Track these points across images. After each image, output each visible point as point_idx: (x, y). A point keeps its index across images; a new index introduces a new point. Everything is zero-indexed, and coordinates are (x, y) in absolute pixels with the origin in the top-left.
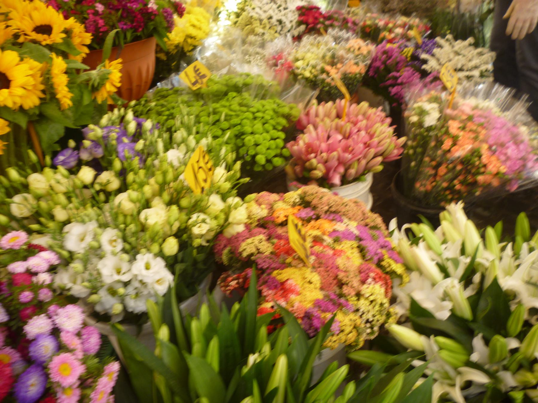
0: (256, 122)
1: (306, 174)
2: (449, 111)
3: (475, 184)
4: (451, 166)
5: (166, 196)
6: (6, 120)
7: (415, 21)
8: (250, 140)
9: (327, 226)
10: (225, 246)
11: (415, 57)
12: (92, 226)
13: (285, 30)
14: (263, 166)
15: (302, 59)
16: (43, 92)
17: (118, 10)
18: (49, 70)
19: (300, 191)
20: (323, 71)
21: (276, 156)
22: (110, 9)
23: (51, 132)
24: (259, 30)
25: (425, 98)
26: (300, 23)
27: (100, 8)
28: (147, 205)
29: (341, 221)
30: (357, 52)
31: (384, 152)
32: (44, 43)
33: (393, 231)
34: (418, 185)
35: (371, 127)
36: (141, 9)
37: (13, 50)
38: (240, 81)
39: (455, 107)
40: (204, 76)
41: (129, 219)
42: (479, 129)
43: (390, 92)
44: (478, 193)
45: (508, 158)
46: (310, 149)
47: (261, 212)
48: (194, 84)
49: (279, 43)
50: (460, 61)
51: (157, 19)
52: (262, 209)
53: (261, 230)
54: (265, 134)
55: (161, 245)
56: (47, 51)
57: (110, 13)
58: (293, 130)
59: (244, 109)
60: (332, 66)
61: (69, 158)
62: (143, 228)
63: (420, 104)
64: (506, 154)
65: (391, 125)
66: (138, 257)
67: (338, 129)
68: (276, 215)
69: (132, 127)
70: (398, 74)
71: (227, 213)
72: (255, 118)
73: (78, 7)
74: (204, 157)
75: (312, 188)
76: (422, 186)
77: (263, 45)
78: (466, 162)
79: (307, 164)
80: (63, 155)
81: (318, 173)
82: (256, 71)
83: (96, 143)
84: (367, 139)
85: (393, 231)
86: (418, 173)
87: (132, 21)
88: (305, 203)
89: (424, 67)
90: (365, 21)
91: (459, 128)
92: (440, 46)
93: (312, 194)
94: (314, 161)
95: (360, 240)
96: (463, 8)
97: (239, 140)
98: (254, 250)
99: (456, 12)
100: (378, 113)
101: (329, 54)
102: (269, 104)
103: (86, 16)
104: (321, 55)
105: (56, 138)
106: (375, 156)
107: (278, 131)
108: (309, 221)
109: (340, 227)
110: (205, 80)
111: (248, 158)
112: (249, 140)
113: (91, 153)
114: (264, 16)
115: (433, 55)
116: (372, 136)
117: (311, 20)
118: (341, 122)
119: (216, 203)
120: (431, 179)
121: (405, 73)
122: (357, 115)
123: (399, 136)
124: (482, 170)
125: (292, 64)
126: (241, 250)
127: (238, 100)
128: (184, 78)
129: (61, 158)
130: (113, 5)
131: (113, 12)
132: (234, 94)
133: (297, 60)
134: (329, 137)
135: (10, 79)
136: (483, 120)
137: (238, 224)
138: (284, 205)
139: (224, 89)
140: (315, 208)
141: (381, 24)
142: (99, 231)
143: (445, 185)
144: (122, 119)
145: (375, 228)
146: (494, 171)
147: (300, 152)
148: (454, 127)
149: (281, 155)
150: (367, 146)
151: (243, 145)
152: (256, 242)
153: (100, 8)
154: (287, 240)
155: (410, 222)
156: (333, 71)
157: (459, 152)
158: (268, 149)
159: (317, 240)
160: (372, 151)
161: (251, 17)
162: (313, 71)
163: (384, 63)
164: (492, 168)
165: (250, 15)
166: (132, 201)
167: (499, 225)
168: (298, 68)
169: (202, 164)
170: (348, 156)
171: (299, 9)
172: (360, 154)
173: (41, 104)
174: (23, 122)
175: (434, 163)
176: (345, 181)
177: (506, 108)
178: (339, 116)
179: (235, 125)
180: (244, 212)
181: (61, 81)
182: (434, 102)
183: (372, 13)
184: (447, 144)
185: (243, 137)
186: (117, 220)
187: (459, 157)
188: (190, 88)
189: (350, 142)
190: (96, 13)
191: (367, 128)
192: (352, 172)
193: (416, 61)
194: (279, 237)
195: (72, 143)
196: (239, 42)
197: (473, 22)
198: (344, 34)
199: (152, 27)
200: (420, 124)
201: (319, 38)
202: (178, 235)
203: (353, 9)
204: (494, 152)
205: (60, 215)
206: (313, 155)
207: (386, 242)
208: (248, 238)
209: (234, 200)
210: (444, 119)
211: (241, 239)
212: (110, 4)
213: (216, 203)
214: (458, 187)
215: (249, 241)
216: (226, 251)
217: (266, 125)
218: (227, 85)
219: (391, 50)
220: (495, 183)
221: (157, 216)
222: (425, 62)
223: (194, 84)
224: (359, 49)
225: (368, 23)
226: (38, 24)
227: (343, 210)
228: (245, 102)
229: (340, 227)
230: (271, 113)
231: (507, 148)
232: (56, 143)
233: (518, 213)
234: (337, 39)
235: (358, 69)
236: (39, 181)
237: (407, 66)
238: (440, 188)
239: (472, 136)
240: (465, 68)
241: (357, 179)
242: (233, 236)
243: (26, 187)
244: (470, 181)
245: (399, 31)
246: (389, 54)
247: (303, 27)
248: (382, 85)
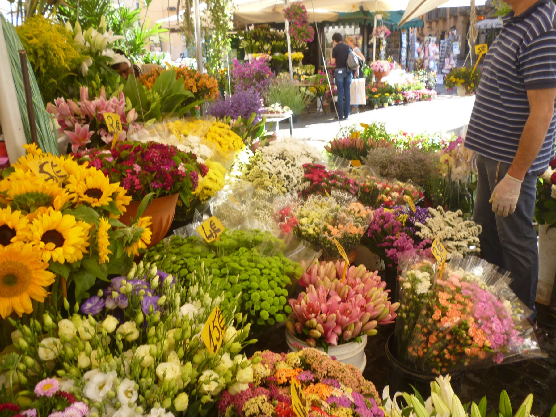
0: (262, 278)
1: (305, 332)
2: (439, 281)
3: (463, 354)
4: (441, 335)
5: (181, 352)
6: (54, 273)
7: (410, 187)
8: (256, 296)
9: (326, 390)
10: (229, 403)
11: (409, 224)
12: (112, 376)
13: (292, 185)
14: (266, 321)
15: (307, 217)
16: (87, 248)
17: (152, 172)
18: (97, 231)
19: (301, 353)
20: (325, 229)
21: (279, 312)
22: (146, 170)
23: (84, 282)
24: (268, 183)
25: (417, 266)
26: (305, 180)
27: (137, 168)
28: (163, 359)
29: (338, 387)
30: (356, 215)
31: (378, 317)
32: (93, 205)
33: (386, 400)
34: (410, 350)
35: (368, 290)
36: (172, 172)
37: (71, 214)
38: (249, 236)
39: (445, 277)
40: (219, 230)
41: (145, 371)
42: (467, 301)
43: (387, 254)
44: (466, 364)
45: (493, 332)
46: (311, 309)
47: (265, 371)
48: (208, 237)
49: (286, 200)
50: (448, 231)
51: (185, 180)
52: (266, 368)
53: (264, 389)
54: (270, 291)
55: (173, 400)
56: (96, 213)
57: (146, 174)
58: (296, 288)
59: (253, 264)
60: (334, 226)
61: (96, 305)
62: (157, 381)
63: (413, 272)
64: (491, 328)
65: (385, 289)
66: (153, 410)
67: (338, 290)
68: (278, 375)
69: (156, 282)
70: (394, 238)
71: (235, 371)
72: (262, 274)
73: (119, 166)
74: (219, 317)
75: (312, 351)
76: (414, 351)
77: (271, 200)
78: (453, 332)
79: (308, 323)
80: (91, 302)
81: (318, 333)
82: (264, 227)
83: (124, 296)
84: (363, 302)
85: (386, 400)
86: (410, 337)
87: (163, 182)
88: (305, 365)
89: (417, 233)
90: (365, 182)
91: (447, 300)
92: (433, 216)
93: (313, 358)
94: (314, 321)
95: (355, 407)
96: (453, 178)
97: (245, 294)
98: (257, 411)
99: (447, 180)
100: (375, 277)
101: (332, 215)
102: (275, 262)
103: (125, 174)
104: (324, 215)
105: (88, 287)
106: (371, 320)
107: (282, 288)
108: (308, 384)
109: (337, 393)
110: (218, 234)
111: (253, 313)
112: (255, 295)
113: (116, 303)
114: (273, 171)
115: (426, 224)
116: (368, 299)
117: (316, 178)
118: (340, 283)
119: (226, 362)
120: (423, 345)
121: (400, 238)
122: (355, 279)
123: (393, 301)
124: (469, 342)
125: (297, 220)
126: (244, 409)
127: (247, 255)
128: (199, 228)
129: (89, 305)
130: (149, 167)
131: (149, 174)
132: (245, 249)
133: (302, 216)
134: (328, 297)
135: (65, 238)
136: (470, 293)
137: (243, 383)
138: (286, 365)
139: (235, 243)
140: (314, 371)
141: (379, 186)
142: (118, 381)
143: (435, 353)
144: (147, 271)
145: (369, 395)
146: (480, 344)
147: (302, 310)
148: (443, 297)
149: (283, 312)
150: (364, 309)
151: (250, 299)
152: (259, 403)
153: (137, 168)
154: (289, 402)
155: (402, 391)
156: (334, 231)
157: (447, 324)
158: (273, 305)
159: (316, 405)
160: (368, 315)
161: (262, 171)
162: (316, 228)
163: (382, 227)
164: (478, 341)
165: (261, 169)
166: (152, 355)
167: (484, 400)
168: (302, 225)
169: (216, 323)
170: (346, 319)
171: (306, 166)
172: (358, 316)
173: (84, 259)
174: (66, 274)
175: (425, 330)
176: (341, 341)
177: (491, 281)
178: (338, 277)
179: (244, 281)
180: (250, 371)
181: (104, 241)
182: (426, 271)
183: (372, 175)
184: (437, 314)
185: (249, 292)
186: (136, 373)
187: (448, 328)
188: (204, 240)
189: (348, 304)
190: (134, 173)
191: (364, 290)
192: (349, 333)
193: (410, 228)
194: (280, 399)
195: (101, 293)
196: (250, 194)
197: (463, 190)
198: (345, 195)
199: (179, 187)
200: (413, 291)
201: (323, 199)
202: (188, 389)
203: (354, 168)
204: (480, 326)
205: (83, 361)
206: (313, 315)
207: (379, 410)
208: (251, 397)
209: (240, 359)
210: (434, 287)
211: (244, 397)
212: (146, 166)
213: (226, 362)
214: (447, 356)
215: (253, 400)
216: (229, 409)
217: (272, 282)
218: (238, 240)
219: (389, 215)
220: (482, 356)
221: (172, 371)
222: (419, 229)
223: (208, 237)
224: (359, 212)
225: (368, 184)
226: (90, 187)
227: (340, 376)
228: (254, 258)
229: (337, 393)
230: (278, 270)
231: (492, 322)
232: (86, 291)
233: (500, 391)
234: (338, 199)
235: (357, 230)
236: (67, 327)
237: (402, 231)
238: (430, 356)
239: (460, 307)
240: (455, 238)
241: (353, 339)
242: (237, 394)
243: (55, 332)
244: (459, 351)
245: (395, 194)
246: (386, 219)
247: (308, 184)
248: (378, 245)
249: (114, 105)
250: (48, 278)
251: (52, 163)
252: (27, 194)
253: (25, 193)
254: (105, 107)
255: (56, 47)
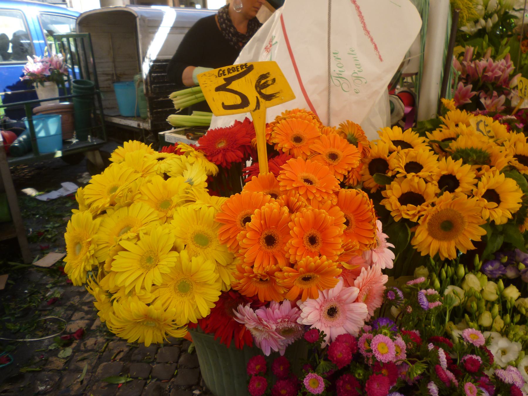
12: (517, 347)
32: (522, 172)
80: (492, 266)
226: (518, 153)
249: (502, 67)
250: (479, 233)
251: (485, 122)
252: (472, 150)
253: (469, 148)
254: (491, 69)
255: (461, 6)
